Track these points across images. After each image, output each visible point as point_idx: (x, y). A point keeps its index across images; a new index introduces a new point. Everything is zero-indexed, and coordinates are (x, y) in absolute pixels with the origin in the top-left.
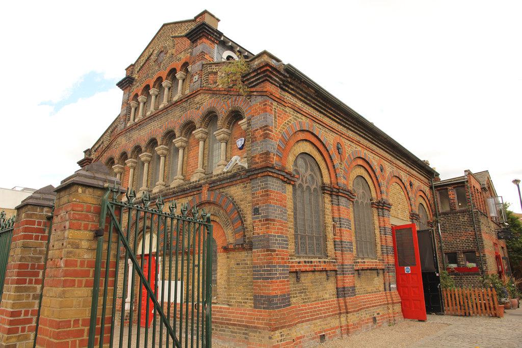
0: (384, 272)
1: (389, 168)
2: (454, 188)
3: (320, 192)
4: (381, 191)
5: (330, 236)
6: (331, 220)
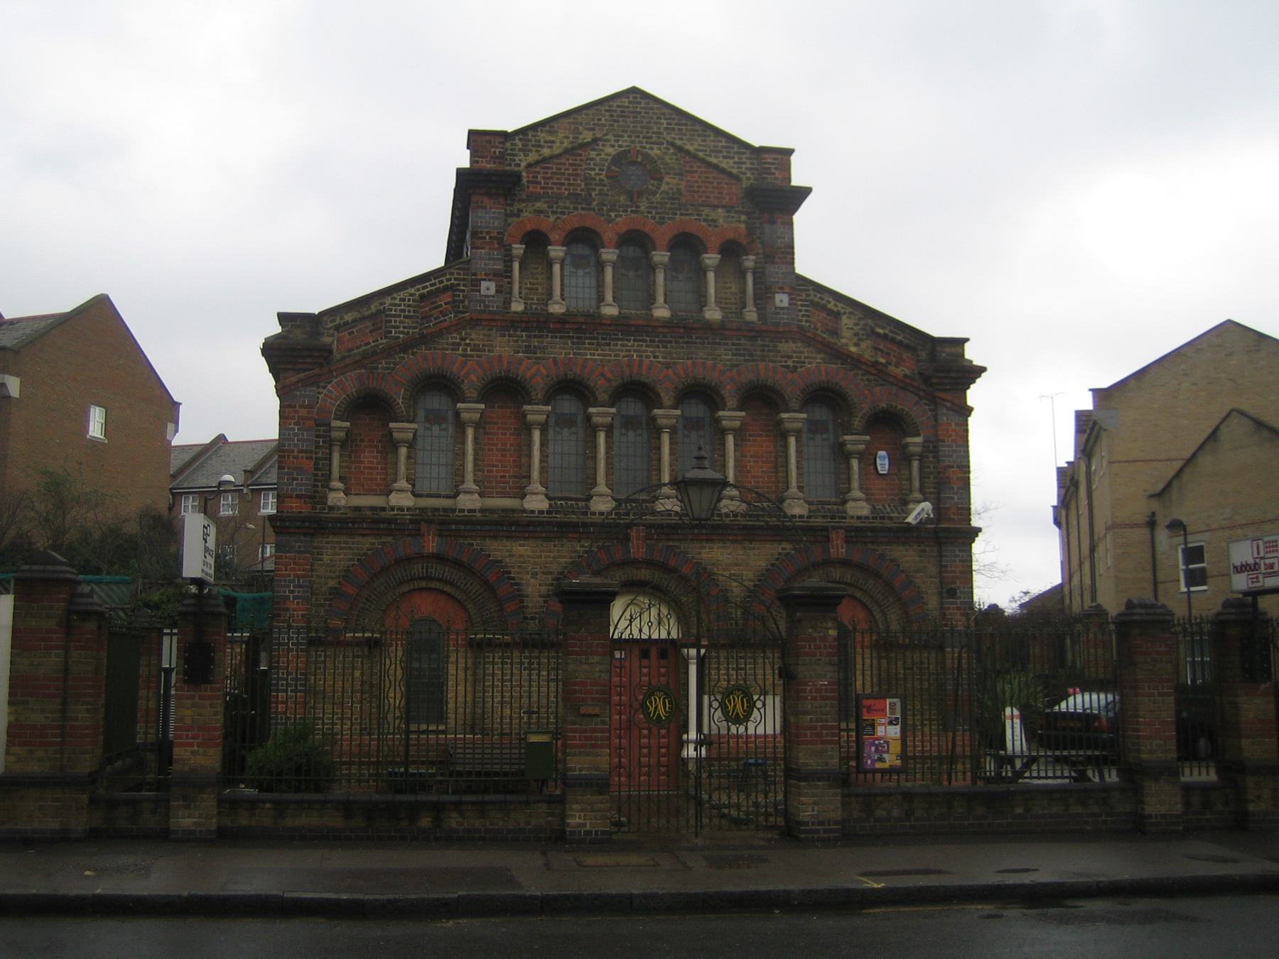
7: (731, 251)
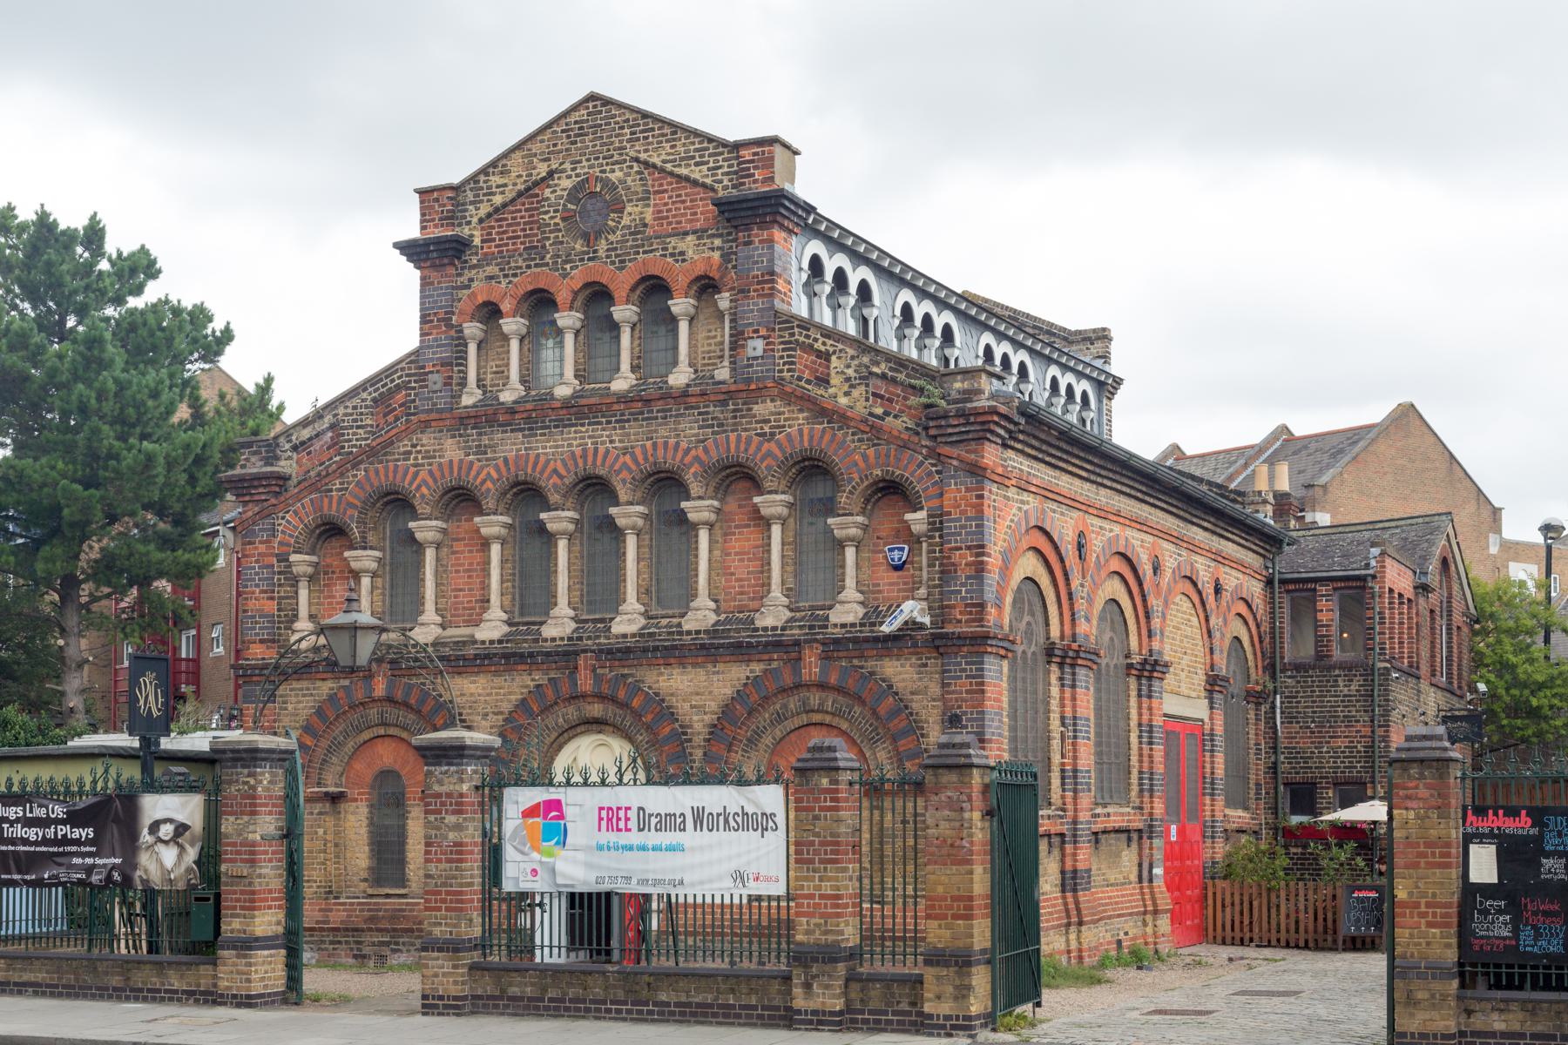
0: (1140, 838)
1: (1171, 558)
2: (1335, 589)
3: (1041, 658)
4: (1150, 631)
5: (1056, 759)
6: (1058, 722)
7: (706, 287)
